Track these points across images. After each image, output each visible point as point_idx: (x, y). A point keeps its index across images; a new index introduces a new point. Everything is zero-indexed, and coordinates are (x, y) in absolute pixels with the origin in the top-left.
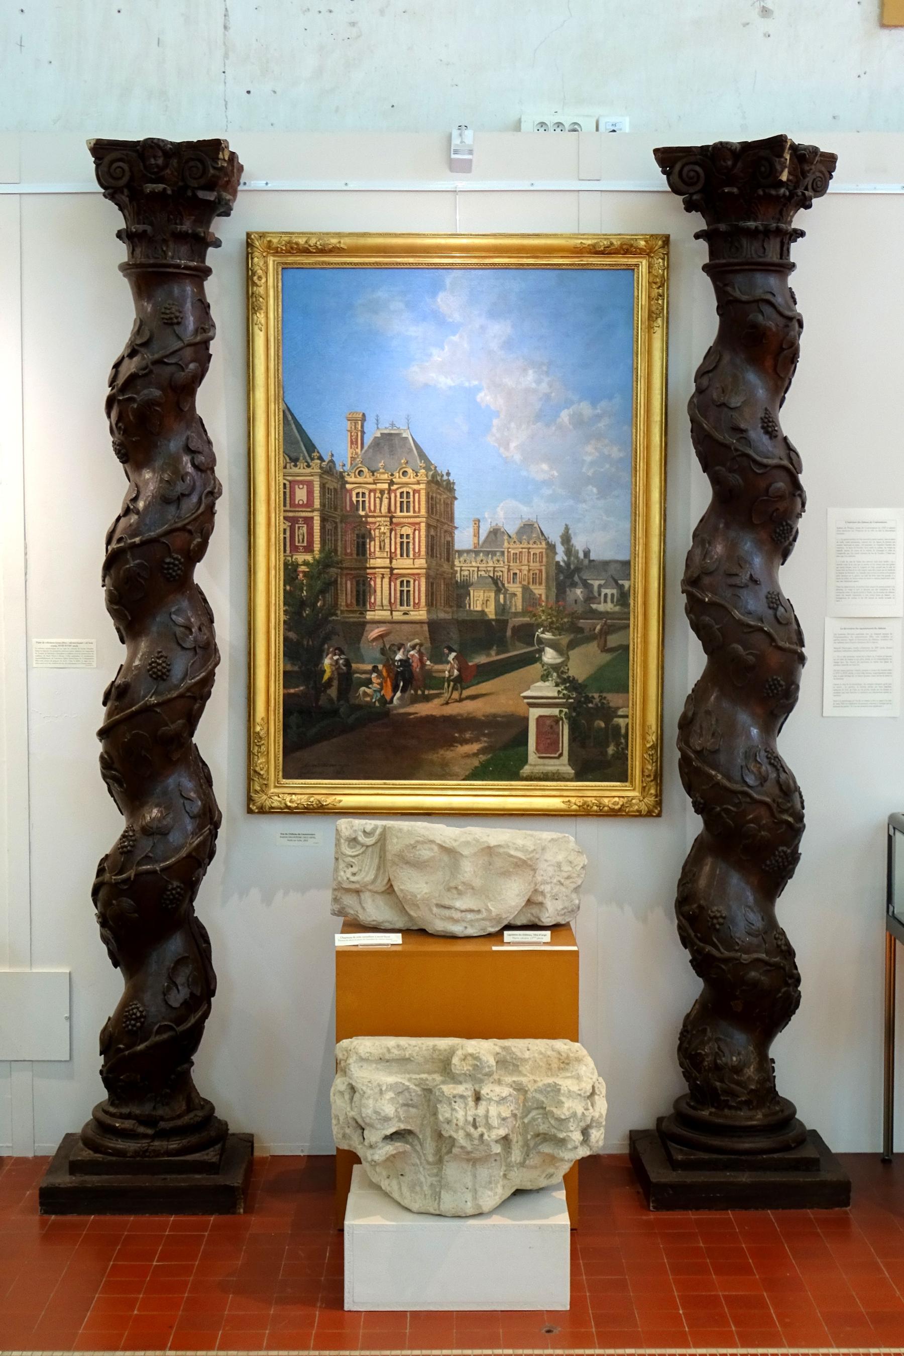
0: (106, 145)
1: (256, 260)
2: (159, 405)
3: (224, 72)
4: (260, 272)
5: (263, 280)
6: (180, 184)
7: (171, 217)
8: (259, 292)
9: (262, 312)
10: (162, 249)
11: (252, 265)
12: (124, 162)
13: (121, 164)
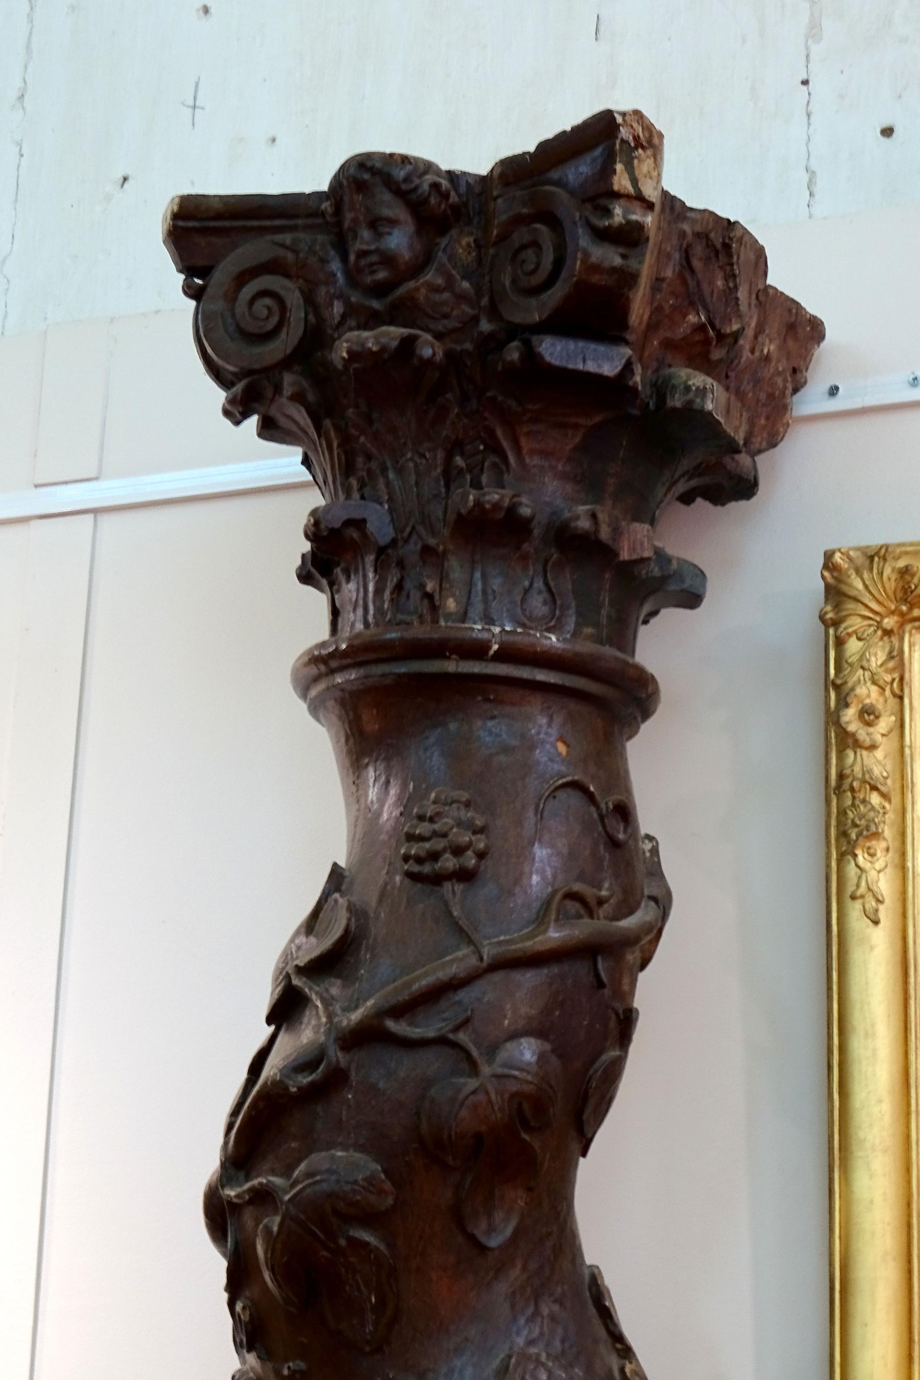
0: (219, 216)
1: (853, 646)
2: (369, 1219)
3: (805, 83)
4: (868, 693)
5: (885, 723)
6: (485, 326)
7: (459, 461)
8: (866, 771)
9: (879, 846)
10: (422, 586)
11: (838, 669)
12: (287, 275)
13: (266, 281)
